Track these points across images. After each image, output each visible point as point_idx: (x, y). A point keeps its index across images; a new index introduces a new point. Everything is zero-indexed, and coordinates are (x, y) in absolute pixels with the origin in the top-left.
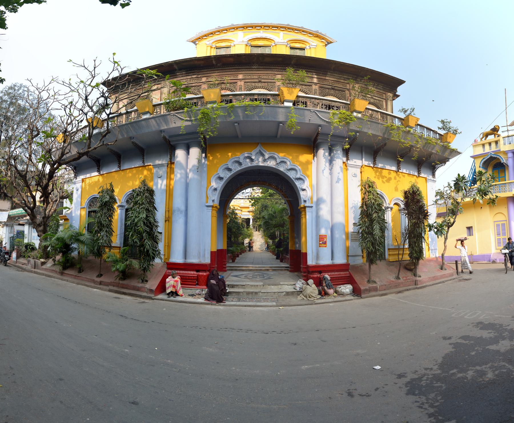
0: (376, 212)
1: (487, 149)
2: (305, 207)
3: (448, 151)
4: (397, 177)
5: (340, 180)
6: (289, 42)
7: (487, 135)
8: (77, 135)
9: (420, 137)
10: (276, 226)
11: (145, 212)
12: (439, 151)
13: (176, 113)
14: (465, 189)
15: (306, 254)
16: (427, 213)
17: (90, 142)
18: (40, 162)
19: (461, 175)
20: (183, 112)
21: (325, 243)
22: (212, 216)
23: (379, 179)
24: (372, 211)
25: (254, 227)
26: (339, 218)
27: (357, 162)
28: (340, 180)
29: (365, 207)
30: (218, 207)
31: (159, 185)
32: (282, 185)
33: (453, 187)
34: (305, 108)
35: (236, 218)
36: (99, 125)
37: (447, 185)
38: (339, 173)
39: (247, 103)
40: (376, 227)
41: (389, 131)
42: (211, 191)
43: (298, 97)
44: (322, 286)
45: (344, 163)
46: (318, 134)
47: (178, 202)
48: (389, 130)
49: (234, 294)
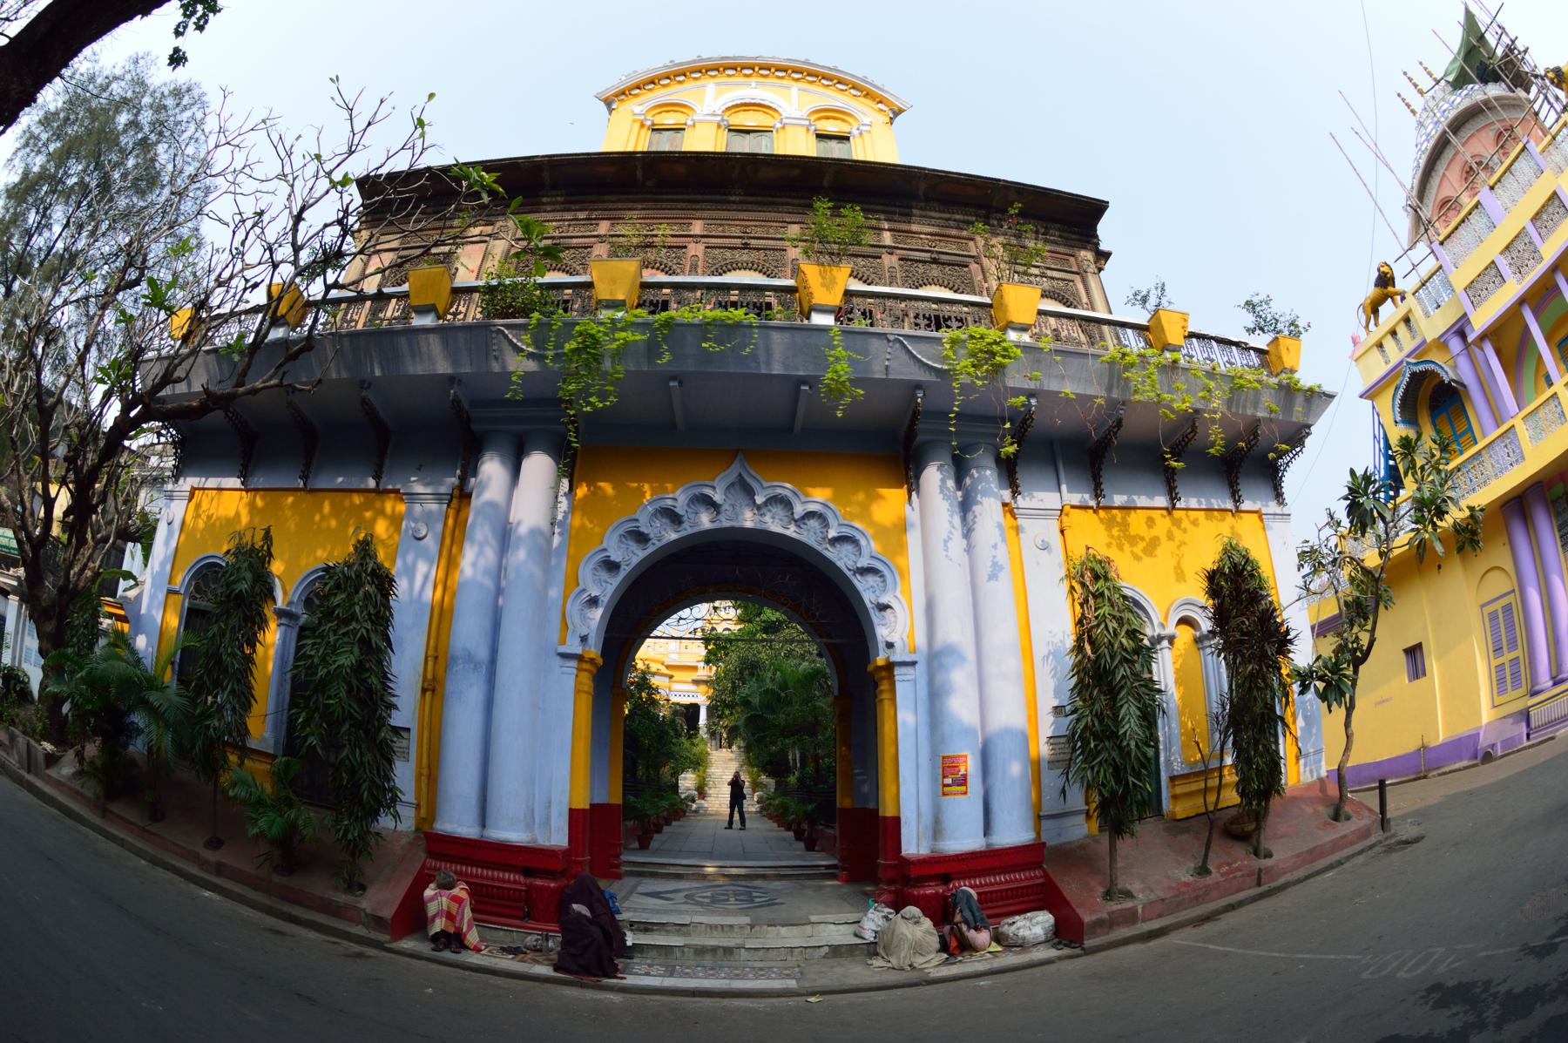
0: (1127, 661)
1: (1394, 354)
2: (890, 667)
3: (1300, 400)
4: (1174, 529)
5: (1001, 568)
6: (813, 117)
7: (1374, 308)
8: (224, 330)
9: (1211, 374)
10: (787, 732)
11: (356, 649)
12: (1274, 407)
13: (507, 326)
14: (1383, 518)
15: (896, 821)
16: (1288, 632)
17: (249, 365)
18: (101, 381)
19: (1359, 472)
20: (524, 327)
21: (963, 781)
22: (577, 692)
23: (1120, 547)
24: (1112, 658)
25: (713, 734)
26: (1008, 713)
27: (1046, 498)
28: (1001, 568)
29: (1088, 647)
30: (600, 661)
31: (416, 583)
32: (818, 601)
33: (1346, 522)
34: (871, 329)
35: (654, 703)
36: (291, 319)
37: (1326, 519)
38: (995, 547)
39: (709, 314)
40: (1129, 712)
41: (1120, 376)
42: (577, 605)
43: (848, 294)
44: (950, 922)
45: (1005, 505)
46: (916, 413)
47: (468, 633)
48: (1117, 371)
49: (654, 953)
